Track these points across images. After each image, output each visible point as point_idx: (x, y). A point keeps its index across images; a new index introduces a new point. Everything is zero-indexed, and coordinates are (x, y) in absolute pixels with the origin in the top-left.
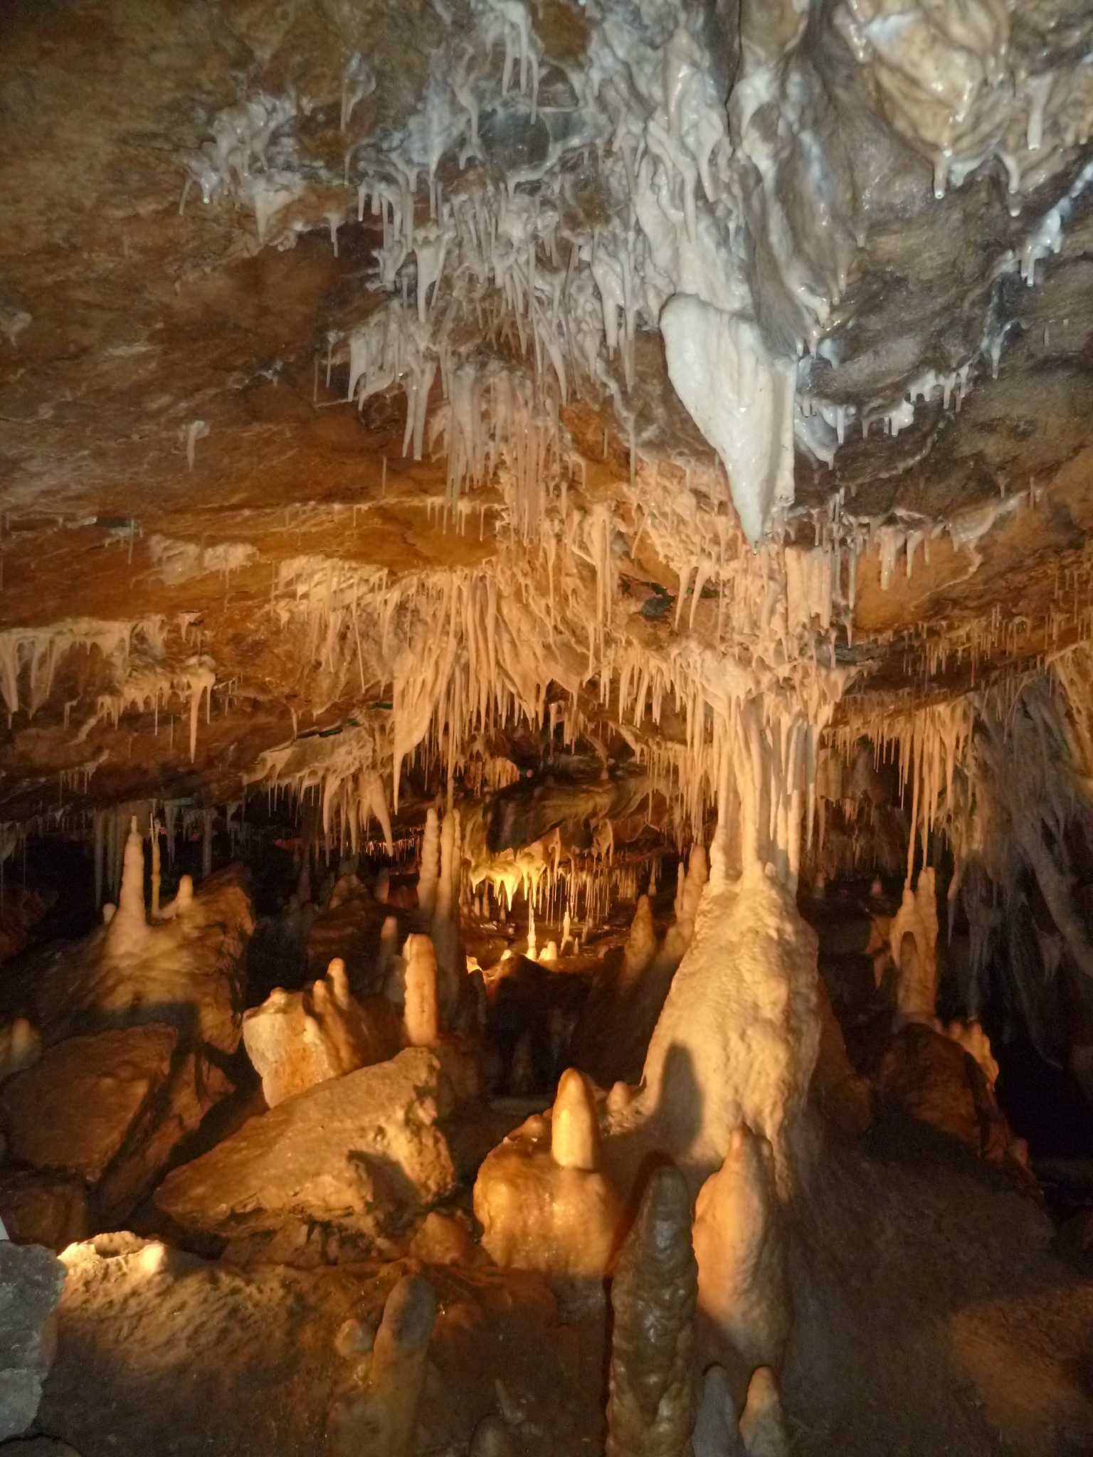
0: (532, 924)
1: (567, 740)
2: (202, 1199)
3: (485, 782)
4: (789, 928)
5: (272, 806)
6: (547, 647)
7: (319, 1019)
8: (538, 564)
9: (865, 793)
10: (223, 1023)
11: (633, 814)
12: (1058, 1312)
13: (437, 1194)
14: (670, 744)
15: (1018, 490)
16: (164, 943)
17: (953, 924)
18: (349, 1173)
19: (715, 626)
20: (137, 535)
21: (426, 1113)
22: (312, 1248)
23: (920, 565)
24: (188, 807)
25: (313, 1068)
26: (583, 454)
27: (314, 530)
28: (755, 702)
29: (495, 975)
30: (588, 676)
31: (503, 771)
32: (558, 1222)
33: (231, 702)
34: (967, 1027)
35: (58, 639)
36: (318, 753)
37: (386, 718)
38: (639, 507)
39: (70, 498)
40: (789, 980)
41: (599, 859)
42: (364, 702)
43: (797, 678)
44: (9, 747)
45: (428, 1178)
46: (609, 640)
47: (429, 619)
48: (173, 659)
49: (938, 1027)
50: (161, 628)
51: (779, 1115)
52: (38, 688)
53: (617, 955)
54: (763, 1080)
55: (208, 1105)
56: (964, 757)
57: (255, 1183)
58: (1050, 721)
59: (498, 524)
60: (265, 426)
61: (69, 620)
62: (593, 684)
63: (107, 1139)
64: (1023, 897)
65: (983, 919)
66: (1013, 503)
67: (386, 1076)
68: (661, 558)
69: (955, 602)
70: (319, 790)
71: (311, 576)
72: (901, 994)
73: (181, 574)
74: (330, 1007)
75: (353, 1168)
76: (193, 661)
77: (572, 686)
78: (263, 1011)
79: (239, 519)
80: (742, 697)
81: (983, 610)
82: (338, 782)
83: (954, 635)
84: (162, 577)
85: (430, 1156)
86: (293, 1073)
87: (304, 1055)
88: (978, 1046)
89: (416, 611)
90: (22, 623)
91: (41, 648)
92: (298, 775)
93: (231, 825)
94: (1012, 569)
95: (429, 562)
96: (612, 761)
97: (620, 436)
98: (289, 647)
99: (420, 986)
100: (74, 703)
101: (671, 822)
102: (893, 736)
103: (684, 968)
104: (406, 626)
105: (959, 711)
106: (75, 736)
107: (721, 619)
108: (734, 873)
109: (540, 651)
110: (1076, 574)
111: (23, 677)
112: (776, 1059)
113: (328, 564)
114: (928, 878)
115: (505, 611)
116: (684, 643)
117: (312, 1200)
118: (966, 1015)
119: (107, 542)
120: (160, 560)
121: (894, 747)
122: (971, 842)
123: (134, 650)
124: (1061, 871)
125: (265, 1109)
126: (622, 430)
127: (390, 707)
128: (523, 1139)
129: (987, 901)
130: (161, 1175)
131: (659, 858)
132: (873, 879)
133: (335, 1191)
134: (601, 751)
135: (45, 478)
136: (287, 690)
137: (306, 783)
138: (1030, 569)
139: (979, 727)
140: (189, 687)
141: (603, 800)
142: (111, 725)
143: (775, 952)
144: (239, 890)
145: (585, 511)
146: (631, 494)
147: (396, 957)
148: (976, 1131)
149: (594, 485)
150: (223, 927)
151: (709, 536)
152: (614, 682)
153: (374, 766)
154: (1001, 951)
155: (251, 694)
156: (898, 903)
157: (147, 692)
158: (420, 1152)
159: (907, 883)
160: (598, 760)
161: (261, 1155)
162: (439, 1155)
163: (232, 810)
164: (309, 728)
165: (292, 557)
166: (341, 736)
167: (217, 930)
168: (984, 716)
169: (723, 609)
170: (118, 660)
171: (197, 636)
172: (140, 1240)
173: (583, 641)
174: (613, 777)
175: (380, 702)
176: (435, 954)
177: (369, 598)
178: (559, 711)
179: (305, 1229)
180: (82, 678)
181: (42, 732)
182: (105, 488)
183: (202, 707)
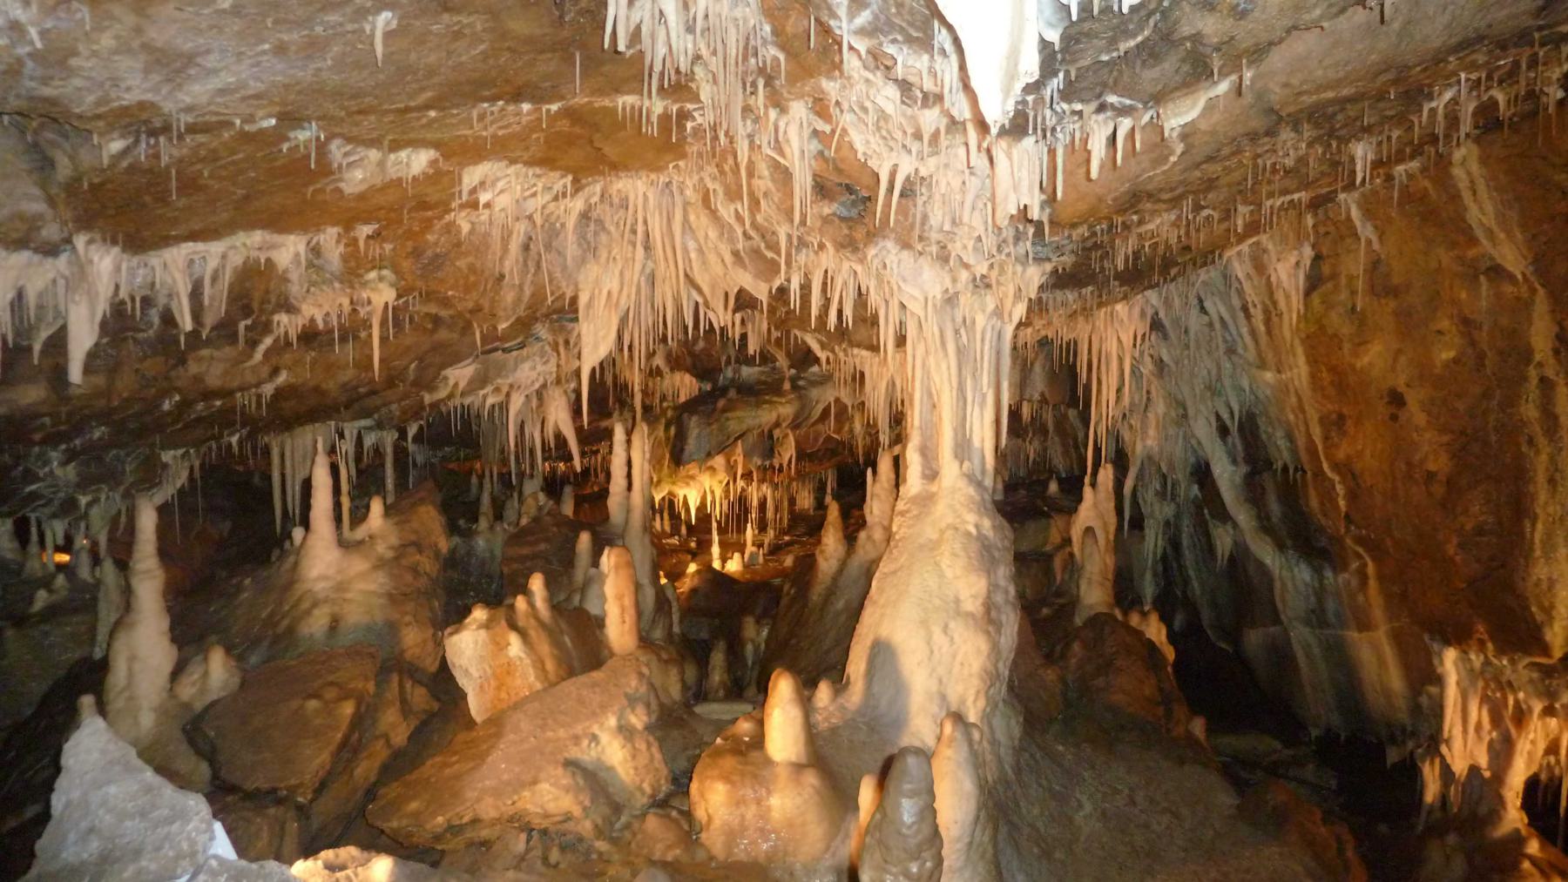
0: (716, 538)
1: (751, 352)
2: (416, 814)
3: (663, 398)
4: (987, 523)
5: (456, 426)
6: (736, 254)
7: (523, 634)
8: (727, 168)
9: (1042, 395)
10: (425, 641)
11: (813, 424)
12: (1248, 871)
13: (653, 796)
14: (856, 351)
15: (1227, 75)
16: (358, 565)
17: (1132, 522)
18: (566, 781)
19: (912, 226)
20: (318, 138)
21: (638, 719)
22: (533, 853)
23: (1131, 151)
24: (370, 429)
25: (518, 682)
26: (783, 48)
27: (500, 133)
28: (951, 300)
29: (685, 585)
30: (777, 283)
31: (685, 385)
32: (776, 815)
33: (411, 319)
34: (1144, 615)
35: (231, 254)
36: (501, 369)
37: (570, 332)
38: (838, 103)
39: (250, 97)
40: (988, 573)
41: (781, 470)
42: (547, 316)
43: (994, 274)
44: (181, 369)
45: (642, 781)
46: (803, 244)
47: (612, 229)
48: (353, 270)
49: (1118, 614)
50: (338, 242)
51: (981, 703)
52: (211, 305)
53: (807, 564)
54: (966, 672)
55: (414, 723)
56: (1142, 353)
57: (471, 794)
58: (1226, 317)
59: (689, 125)
60: (455, 19)
61: (241, 234)
62: (783, 291)
63: (316, 759)
64: (1195, 489)
65: (1158, 512)
66: (1223, 87)
67: (594, 685)
68: (860, 156)
69: (1150, 196)
70: (504, 407)
71: (494, 183)
72: (1083, 587)
73: (362, 181)
74: (532, 621)
75: (569, 774)
76: (373, 275)
77: (761, 291)
78: (465, 628)
79: (424, 121)
80: (939, 297)
81: (1175, 202)
82: (522, 399)
83: (1142, 229)
84: (342, 185)
85: (643, 760)
86: (498, 688)
87: (509, 668)
88: (1155, 631)
89: (599, 222)
90: (193, 237)
91: (213, 263)
92: (482, 393)
93: (411, 447)
94: (1210, 159)
95: (616, 167)
96: (793, 371)
97: (832, 23)
98: (470, 259)
99: (620, 598)
100: (249, 322)
101: (851, 431)
102: (1071, 336)
103: (884, 568)
104: (590, 236)
105: (1137, 310)
106: (250, 357)
107: (919, 216)
108: (931, 475)
109: (728, 258)
110: (1268, 164)
111: (196, 294)
112: (979, 651)
113: (512, 170)
114: (1106, 474)
115: (692, 218)
116: (881, 244)
117: (531, 808)
118: (1142, 604)
119: (285, 147)
120: (340, 166)
121: (1072, 348)
122: (1146, 442)
123: (310, 265)
124: (1234, 462)
125: (471, 723)
126: (834, 15)
127: (576, 320)
128: (736, 739)
129: (1162, 495)
130: (371, 794)
131: (847, 468)
132: (1050, 478)
133: (552, 797)
134: (782, 361)
135: (223, 74)
136: (470, 305)
137: (490, 401)
138: (1227, 158)
139: (1156, 325)
140: (369, 302)
141: (787, 410)
142: (288, 344)
143: (974, 547)
144: (430, 508)
145: (783, 110)
146: (830, 87)
147: (593, 571)
148: (1161, 711)
149: (792, 79)
150: (418, 546)
151: (910, 131)
152: (806, 288)
153: (558, 382)
154: (1175, 544)
155: (433, 309)
156: (1079, 499)
157: (326, 308)
158: (634, 757)
159: (1087, 480)
160: (780, 371)
161: (473, 768)
162: (652, 759)
163: (412, 431)
164: (493, 343)
165: (476, 163)
166: (525, 352)
167: (412, 550)
168: (1162, 315)
169: (920, 207)
170: (294, 276)
171: (376, 250)
172: (366, 854)
173: (775, 247)
174: (795, 387)
175: (565, 313)
176: (631, 564)
177: (552, 206)
178: (743, 322)
179: (523, 836)
180: (257, 295)
181: (216, 353)
182: (286, 87)
183: (384, 323)
